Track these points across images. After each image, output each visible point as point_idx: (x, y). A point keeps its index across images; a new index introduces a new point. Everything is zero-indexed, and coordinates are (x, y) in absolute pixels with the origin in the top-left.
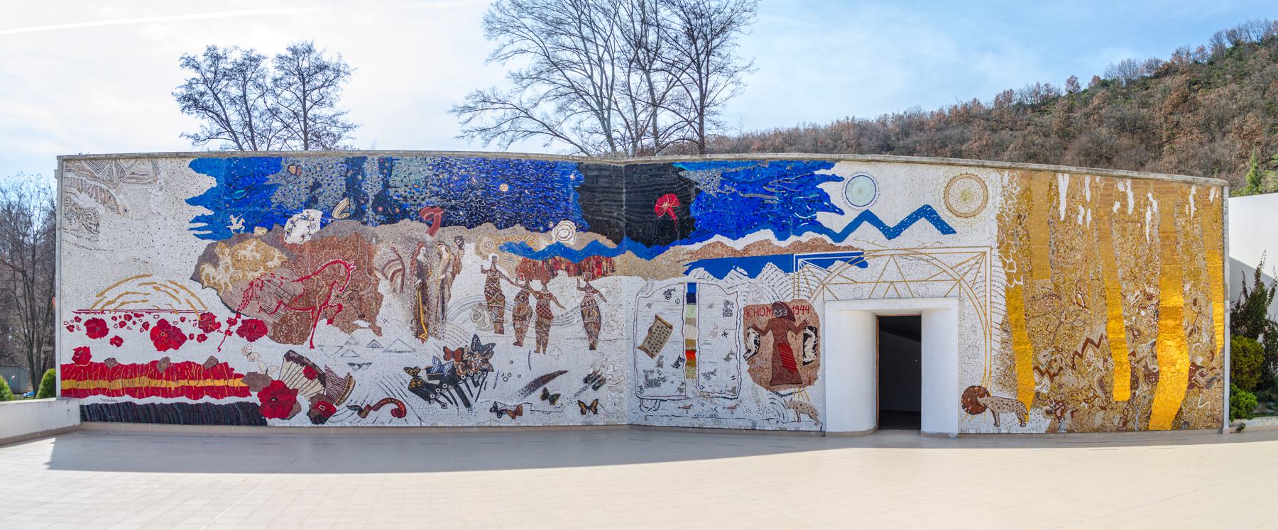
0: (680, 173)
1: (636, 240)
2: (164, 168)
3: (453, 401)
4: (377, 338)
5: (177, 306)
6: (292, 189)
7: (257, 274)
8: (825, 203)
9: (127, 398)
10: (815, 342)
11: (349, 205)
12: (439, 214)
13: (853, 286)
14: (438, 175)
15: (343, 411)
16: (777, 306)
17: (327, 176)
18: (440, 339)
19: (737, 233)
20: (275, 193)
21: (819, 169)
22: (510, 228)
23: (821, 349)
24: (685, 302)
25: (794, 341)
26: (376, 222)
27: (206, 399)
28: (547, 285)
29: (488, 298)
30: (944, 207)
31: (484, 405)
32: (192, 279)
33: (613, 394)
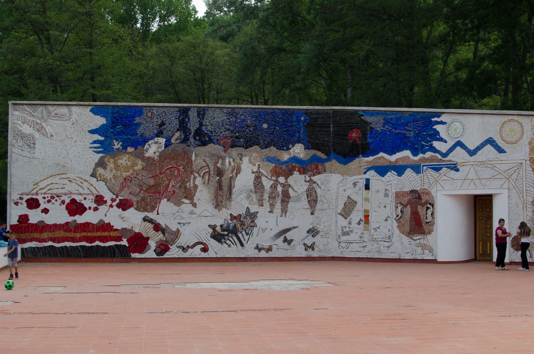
0: (362, 117)
1: (338, 154)
2: (75, 111)
3: (234, 243)
4: (194, 209)
5: (81, 191)
6: (149, 126)
7: (128, 174)
8: (438, 137)
9: (50, 243)
10: (432, 211)
11: (181, 136)
12: (230, 141)
13: (452, 182)
14: (229, 119)
15: (174, 249)
16: (413, 192)
17: (168, 119)
18: (228, 209)
19: (392, 152)
20: (140, 128)
21: (434, 118)
22: (268, 149)
23: (435, 215)
24: (364, 189)
25: (421, 210)
26: (195, 145)
27: (97, 243)
28: (288, 179)
29: (255, 187)
30: (500, 138)
31: (251, 245)
32: (91, 176)
33: (324, 240)
